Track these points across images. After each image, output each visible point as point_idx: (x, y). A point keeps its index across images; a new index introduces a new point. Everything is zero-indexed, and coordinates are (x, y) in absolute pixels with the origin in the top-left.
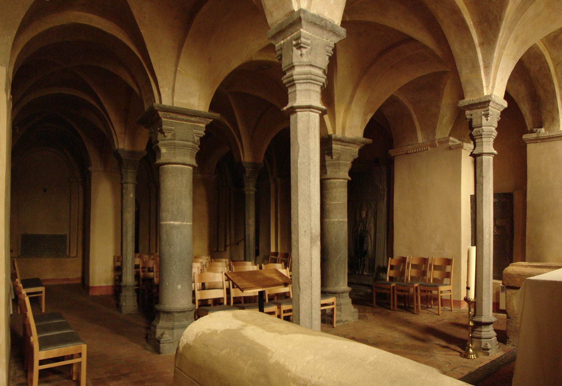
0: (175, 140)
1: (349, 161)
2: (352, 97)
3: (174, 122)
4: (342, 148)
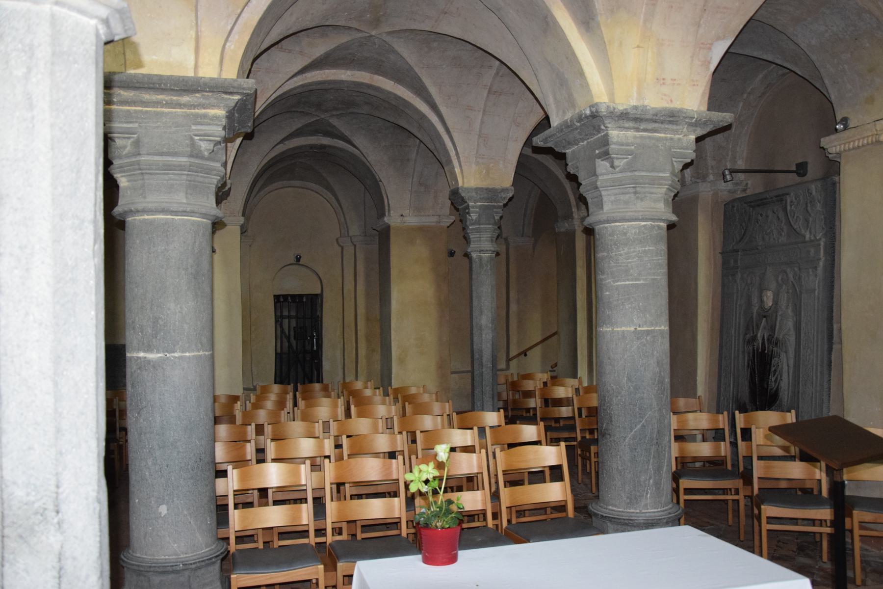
0: (139, 154)
1: (663, 171)
3: (136, 111)
4: (641, 137)
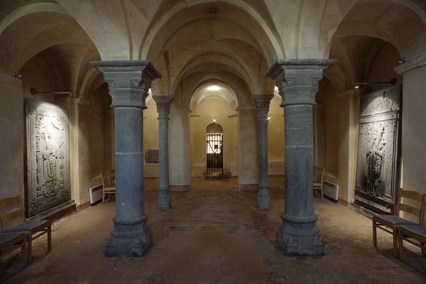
2: (299, 17)
4: (298, 72)
